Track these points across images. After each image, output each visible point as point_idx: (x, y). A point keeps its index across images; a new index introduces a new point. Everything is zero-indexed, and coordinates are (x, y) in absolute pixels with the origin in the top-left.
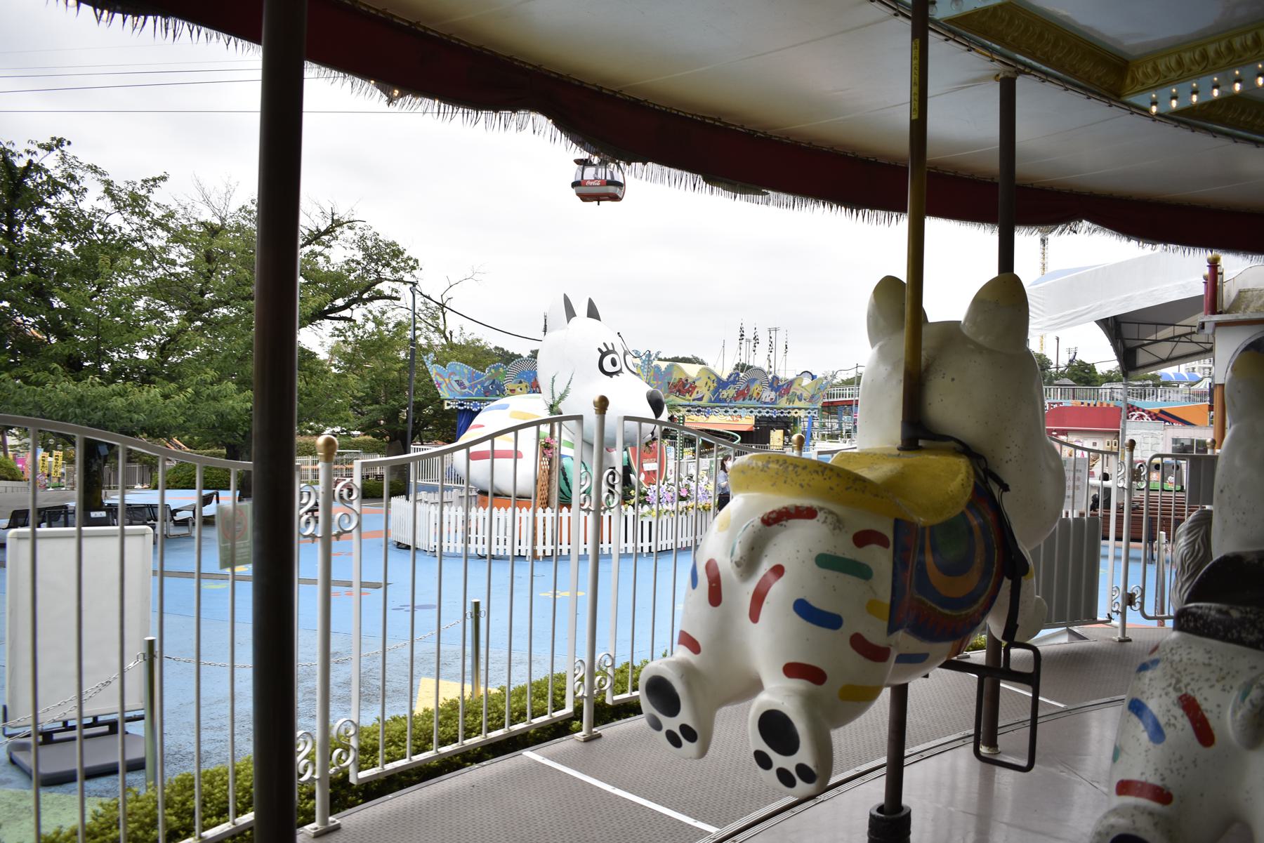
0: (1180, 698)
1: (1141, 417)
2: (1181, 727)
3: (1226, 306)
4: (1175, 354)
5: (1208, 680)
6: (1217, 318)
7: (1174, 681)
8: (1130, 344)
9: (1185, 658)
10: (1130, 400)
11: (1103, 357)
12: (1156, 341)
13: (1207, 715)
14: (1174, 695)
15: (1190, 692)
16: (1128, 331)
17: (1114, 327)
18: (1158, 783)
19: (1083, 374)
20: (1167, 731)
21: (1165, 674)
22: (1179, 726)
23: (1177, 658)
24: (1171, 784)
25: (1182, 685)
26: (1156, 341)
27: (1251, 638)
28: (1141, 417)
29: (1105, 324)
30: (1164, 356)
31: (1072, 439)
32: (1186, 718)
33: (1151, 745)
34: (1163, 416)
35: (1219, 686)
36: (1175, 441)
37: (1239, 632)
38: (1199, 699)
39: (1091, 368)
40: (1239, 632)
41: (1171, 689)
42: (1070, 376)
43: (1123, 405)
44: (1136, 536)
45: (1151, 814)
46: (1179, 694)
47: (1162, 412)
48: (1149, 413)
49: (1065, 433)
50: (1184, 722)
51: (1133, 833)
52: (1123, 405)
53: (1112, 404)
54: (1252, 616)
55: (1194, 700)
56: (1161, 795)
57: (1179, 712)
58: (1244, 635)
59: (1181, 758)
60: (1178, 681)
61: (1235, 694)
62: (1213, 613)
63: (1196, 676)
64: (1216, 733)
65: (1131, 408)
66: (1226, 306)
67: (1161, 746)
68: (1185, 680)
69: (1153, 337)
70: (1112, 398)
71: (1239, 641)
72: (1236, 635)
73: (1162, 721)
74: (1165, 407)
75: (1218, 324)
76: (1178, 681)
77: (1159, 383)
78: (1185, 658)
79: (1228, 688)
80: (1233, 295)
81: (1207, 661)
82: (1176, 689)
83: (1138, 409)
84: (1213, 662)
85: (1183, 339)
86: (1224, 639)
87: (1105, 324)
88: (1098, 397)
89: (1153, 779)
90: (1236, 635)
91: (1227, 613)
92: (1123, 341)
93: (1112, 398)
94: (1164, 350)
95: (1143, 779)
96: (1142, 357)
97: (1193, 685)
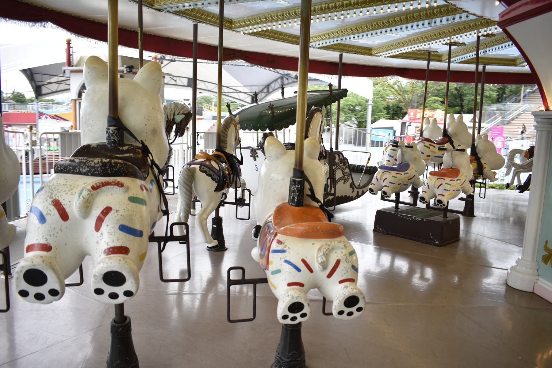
0: (53, 201)
1: (46, 118)
2: (54, 215)
3: (75, 63)
4: (59, 89)
5: (65, 191)
6: (71, 68)
7: (50, 194)
8: (39, 84)
9: (55, 183)
10: (40, 110)
11: (29, 92)
12: (51, 83)
13: (64, 207)
14: (50, 200)
15: (57, 198)
16: (37, 77)
17: (30, 74)
18: (45, 242)
19: (19, 99)
20: (47, 217)
21: (46, 192)
22: (52, 214)
23: (51, 184)
24: (51, 242)
25: (53, 195)
26: (51, 83)
27: (85, 171)
28: (46, 118)
29: (25, 71)
30: (54, 90)
31: (14, 128)
32: (56, 210)
33: (40, 225)
34: (56, 117)
35: (70, 193)
36: (62, 128)
37: (79, 169)
38: (61, 200)
39: (23, 96)
40: (79, 169)
41: (48, 198)
42: (13, 99)
43: (36, 112)
44: (45, 171)
45: (41, 257)
46: (52, 200)
47: (55, 115)
48: (50, 116)
49: (10, 125)
50: (55, 212)
51: (33, 267)
52: (36, 112)
53: (33, 112)
54: (84, 161)
55: (59, 201)
56: (46, 248)
57: (52, 207)
58: (81, 170)
59: (54, 229)
60: (52, 194)
61: (77, 195)
62: (68, 162)
63: (59, 191)
64: (69, 214)
65: (41, 114)
66: (75, 63)
67: (44, 225)
68: (55, 193)
69: (49, 81)
70: (33, 109)
71: (80, 173)
72: (78, 170)
73: (44, 213)
74: (57, 114)
75: (72, 71)
76: (52, 194)
77: (54, 103)
78: (55, 183)
79: (74, 193)
80: (78, 58)
81: (65, 183)
82: (50, 198)
83: (45, 114)
84: (67, 183)
85: (62, 83)
86: (73, 173)
87: (25, 71)
88: (26, 109)
89: (43, 241)
90: (78, 170)
91: (73, 161)
92: (35, 81)
93: (33, 109)
94: (54, 87)
95: (37, 242)
96: (44, 90)
97: (59, 195)
